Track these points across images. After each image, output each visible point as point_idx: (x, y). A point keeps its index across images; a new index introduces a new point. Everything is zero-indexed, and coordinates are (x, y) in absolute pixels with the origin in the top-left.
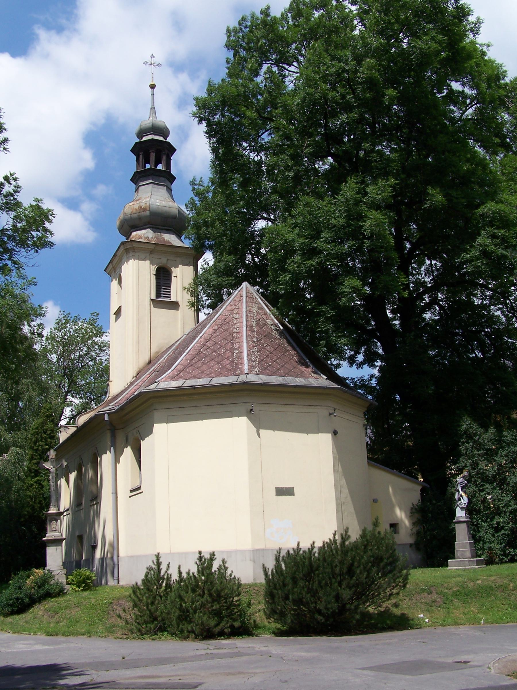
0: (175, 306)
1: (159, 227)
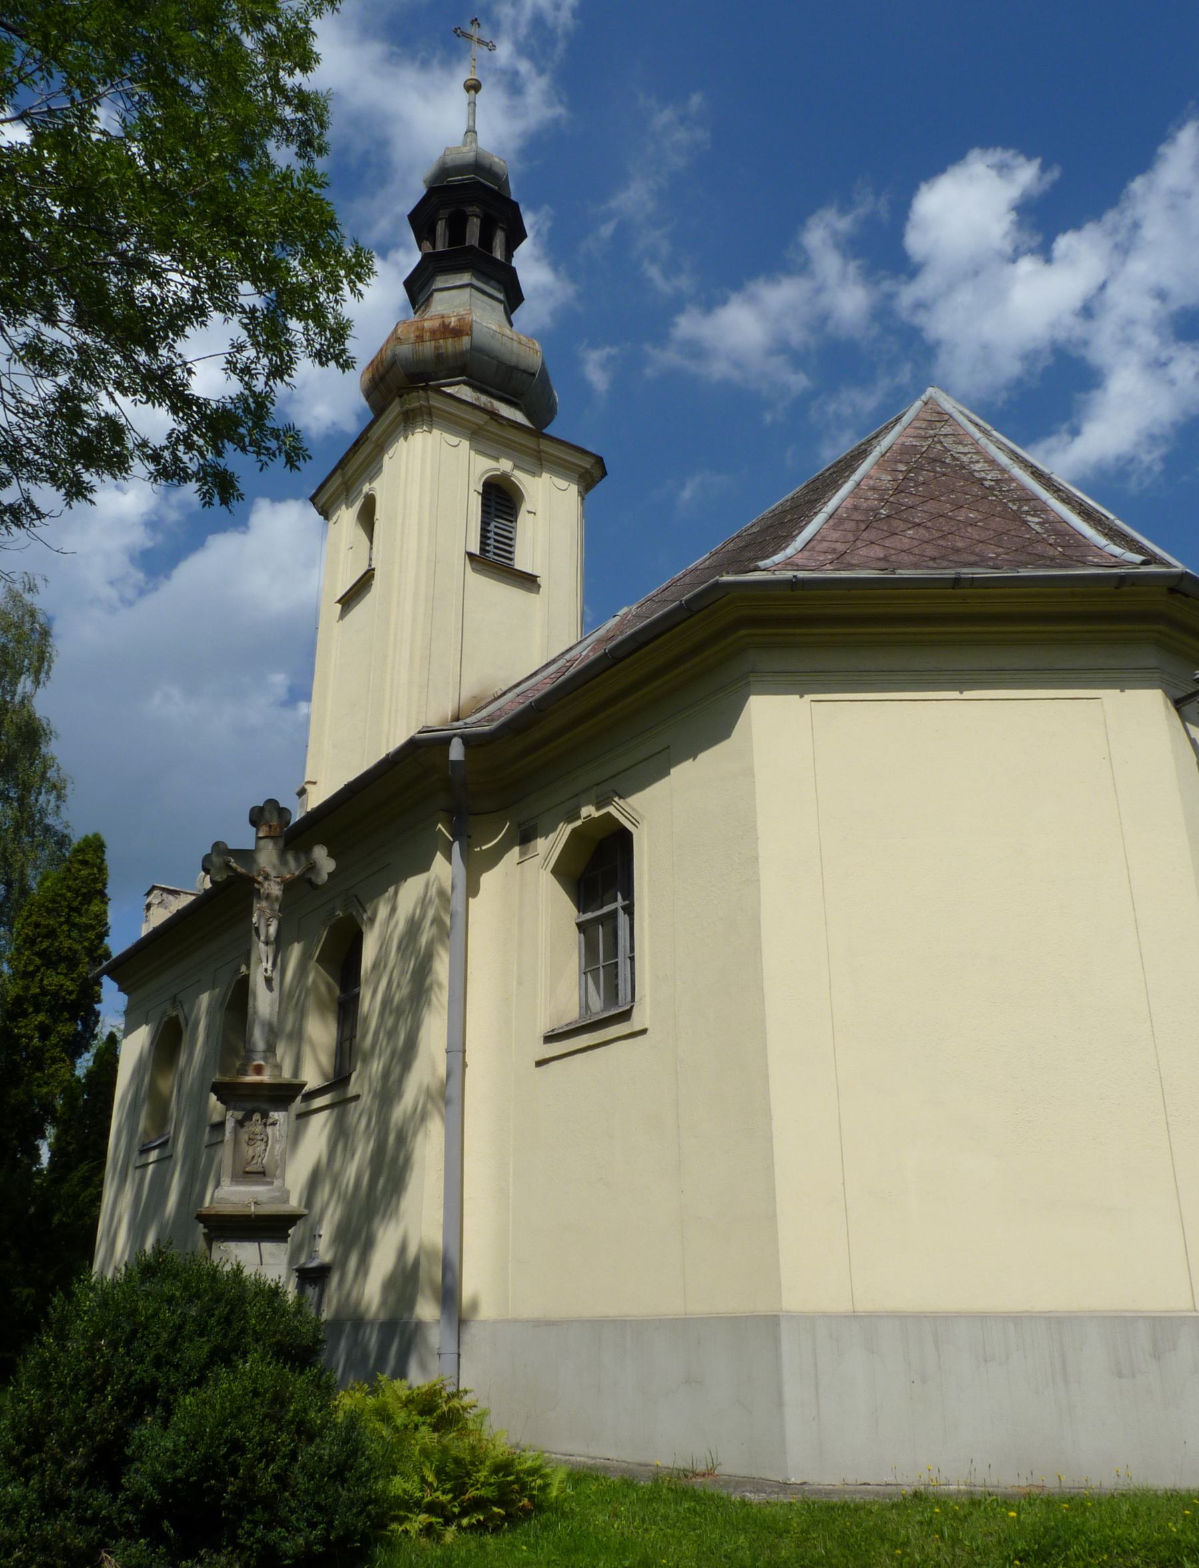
0: (528, 581)
1: (490, 389)
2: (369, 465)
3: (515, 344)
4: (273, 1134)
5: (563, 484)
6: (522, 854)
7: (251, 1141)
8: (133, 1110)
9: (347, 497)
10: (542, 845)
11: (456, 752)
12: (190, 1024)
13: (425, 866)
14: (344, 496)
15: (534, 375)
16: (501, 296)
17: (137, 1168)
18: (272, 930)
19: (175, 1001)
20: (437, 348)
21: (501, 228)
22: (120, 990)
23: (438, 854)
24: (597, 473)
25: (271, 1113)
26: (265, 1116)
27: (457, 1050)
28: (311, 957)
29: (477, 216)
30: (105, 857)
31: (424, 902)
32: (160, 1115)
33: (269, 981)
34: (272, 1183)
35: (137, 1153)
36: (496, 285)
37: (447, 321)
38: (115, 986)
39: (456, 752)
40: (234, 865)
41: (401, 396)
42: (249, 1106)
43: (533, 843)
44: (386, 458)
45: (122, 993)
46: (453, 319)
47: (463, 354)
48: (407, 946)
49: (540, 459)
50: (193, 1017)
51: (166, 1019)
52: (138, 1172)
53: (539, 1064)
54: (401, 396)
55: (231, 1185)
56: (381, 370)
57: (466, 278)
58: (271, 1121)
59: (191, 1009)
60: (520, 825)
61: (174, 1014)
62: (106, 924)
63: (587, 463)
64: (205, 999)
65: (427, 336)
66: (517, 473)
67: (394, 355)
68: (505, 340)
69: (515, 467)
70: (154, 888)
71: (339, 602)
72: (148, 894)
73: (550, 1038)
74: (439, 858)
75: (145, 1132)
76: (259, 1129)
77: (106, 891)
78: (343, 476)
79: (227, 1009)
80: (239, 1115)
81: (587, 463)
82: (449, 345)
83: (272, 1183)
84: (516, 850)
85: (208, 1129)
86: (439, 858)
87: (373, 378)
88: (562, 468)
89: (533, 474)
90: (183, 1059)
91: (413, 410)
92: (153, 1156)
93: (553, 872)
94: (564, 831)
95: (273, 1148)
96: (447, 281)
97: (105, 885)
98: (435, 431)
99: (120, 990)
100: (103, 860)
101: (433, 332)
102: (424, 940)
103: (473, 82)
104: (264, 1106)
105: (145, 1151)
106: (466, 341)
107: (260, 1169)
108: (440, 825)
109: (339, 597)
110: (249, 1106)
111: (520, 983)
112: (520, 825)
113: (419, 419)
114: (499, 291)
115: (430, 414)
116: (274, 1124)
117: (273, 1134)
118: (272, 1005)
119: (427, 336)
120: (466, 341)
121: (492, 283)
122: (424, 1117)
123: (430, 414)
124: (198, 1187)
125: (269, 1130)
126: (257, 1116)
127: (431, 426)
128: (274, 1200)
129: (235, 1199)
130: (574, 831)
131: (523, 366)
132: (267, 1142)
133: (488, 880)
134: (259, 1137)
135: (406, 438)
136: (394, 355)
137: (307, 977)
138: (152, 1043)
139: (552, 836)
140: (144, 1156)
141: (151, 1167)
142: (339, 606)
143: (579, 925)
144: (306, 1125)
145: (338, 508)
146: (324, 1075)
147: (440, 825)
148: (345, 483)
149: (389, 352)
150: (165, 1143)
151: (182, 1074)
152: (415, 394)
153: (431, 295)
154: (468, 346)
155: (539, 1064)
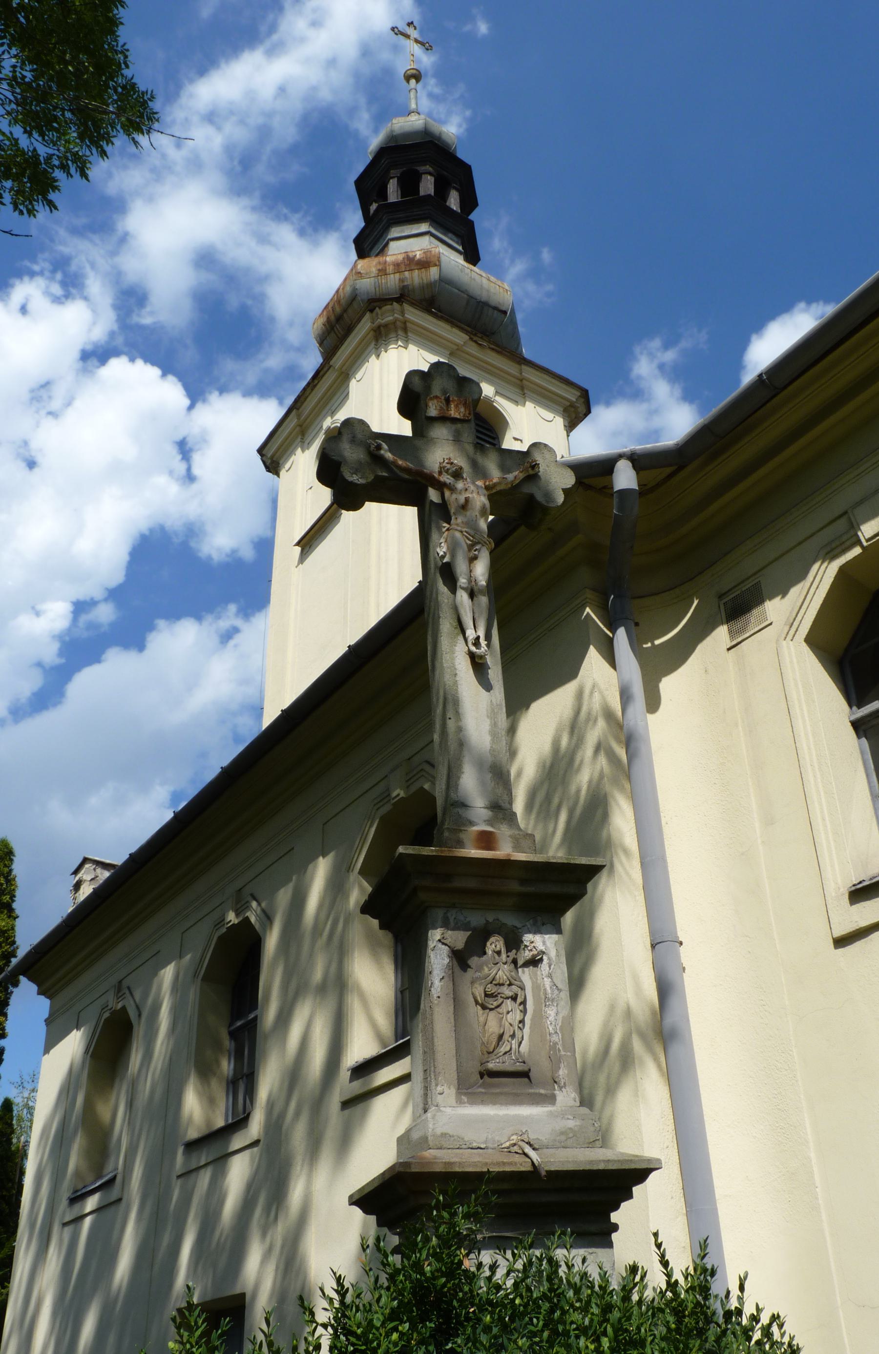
2: (334, 394)
3: (485, 281)
4: (537, 987)
5: (549, 415)
6: (732, 634)
7: (489, 1001)
8: (60, 1143)
9: (302, 441)
10: (775, 609)
11: (625, 478)
12: (145, 1014)
13: (569, 671)
14: (299, 439)
15: (505, 313)
16: (460, 248)
17: (65, 1225)
18: (481, 570)
19: (119, 989)
20: (401, 280)
21: (457, 190)
22: (39, 993)
23: (592, 647)
24: (582, 409)
25: (528, 938)
26: (514, 943)
27: (662, 941)
28: (349, 869)
29: (430, 174)
30: (13, 867)
31: (575, 726)
32: (100, 1144)
33: (478, 665)
34: (551, 1099)
35: (65, 1202)
36: (455, 239)
37: (411, 255)
38: (34, 988)
39: (625, 478)
40: (389, 456)
41: (372, 311)
42: (477, 919)
43: (755, 612)
44: (353, 383)
45: (42, 997)
46: (418, 253)
47: (431, 285)
48: (548, 799)
49: (522, 388)
50: (150, 1001)
51: (107, 1015)
52: (68, 1230)
53: (841, 942)
54: (372, 311)
55: (460, 1102)
56: (338, 310)
57: (424, 227)
58: (527, 955)
59: (146, 995)
60: (720, 596)
61: (119, 1006)
62: (14, 942)
63: (572, 395)
64: (168, 973)
65: (390, 269)
66: (498, 399)
67: (354, 290)
68: (474, 275)
69: (497, 393)
70: (85, 860)
71: (298, 544)
72: (76, 872)
73: (860, 893)
74: (593, 658)
75: (77, 1174)
76: (503, 972)
77: (14, 905)
78: (299, 416)
79: (204, 979)
80: (459, 939)
81: (572, 395)
82: (415, 278)
83: (551, 1099)
84: (721, 633)
85: (181, 1150)
86: (593, 658)
87: (328, 320)
88: (546, 399)
89: (516, 403)
90: (135, 1059)
91: (386, 326)
92: (91, 1203)
93: (809, 640)
94: (823, 576)
95: (539, 1016)
96: (403, 231)
97: (12, 897)
98: (411, 347)
99: (39, 993)
100: (11, 871)
101: (397, 265)
102: (584, 778)
103: (414, 72)
104: (510, 920)
105: (77, 1198)
106: (434, 273)
107: (519, 1067)
108: (588, 610)
109: (297, 538)
110: (477, 919)
111: (769, 821)
112: (720, 596)
113: (393, 335)
114: (457, 243)
115: (405, 330)
116: (534, 962)
117: (537, 987)
118: (492, 714)
119: (390, 269)
120: (434, 273)
121: (450, 235)
122: (627, 1061)
123: (405, 330)
124: (166, 1239)
125: (526, 975)
126: (495, 944)
127: (407, 341)
128: (566, 1138)
129: (476, 1137)
130: (842, 570)
131: (493, 303)
132: (524, 1003)
133: (668, 685)
134: (507, 991)
135: (378, 356)
136: (354, 290)
137: (347, 897)
138: (86, 1051)
139: (796, 592)
140: (77, 1206)
141: (88, 1221)
142: (298, 549)
143: (857, 725)
144: (364, 1115)
145: (293, 452)
146: (380, 1037)
147: (588, 610)
148: (301, 426)
149: (348, 289)
150: (111, 1181)
151: (134, 1084)
152: (388, 307)
153: (387, 245)
154: (437, 277)
155: (841, 942)
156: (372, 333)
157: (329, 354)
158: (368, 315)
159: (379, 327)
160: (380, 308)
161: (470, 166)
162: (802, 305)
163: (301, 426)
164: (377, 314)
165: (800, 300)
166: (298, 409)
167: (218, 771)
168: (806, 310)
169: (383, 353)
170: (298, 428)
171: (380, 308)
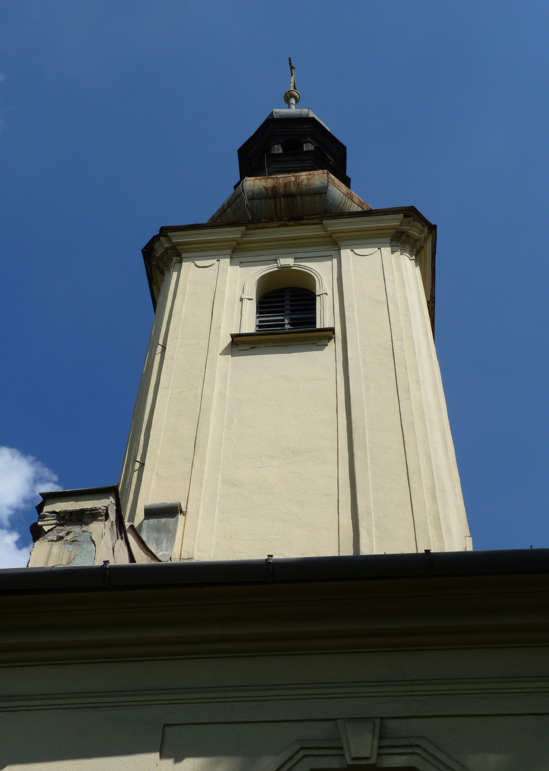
54: (405, 216)
70: (165, 725)
91: (408, 236)
152: (420, 225)
156: (394, 231)
157: (220, 220)
158: (401, 216)
159: (403, 232)
160: (414, 220)
161: (413, 207)
162: (31, 458)
163: (238, 244)
164: (409, 222)
165: (33, 455)
166: (247, 229)
167: (527, 547)
168: (32, 464)
169: (398, 253)
170: (235, 243)
171: (414, 220)
